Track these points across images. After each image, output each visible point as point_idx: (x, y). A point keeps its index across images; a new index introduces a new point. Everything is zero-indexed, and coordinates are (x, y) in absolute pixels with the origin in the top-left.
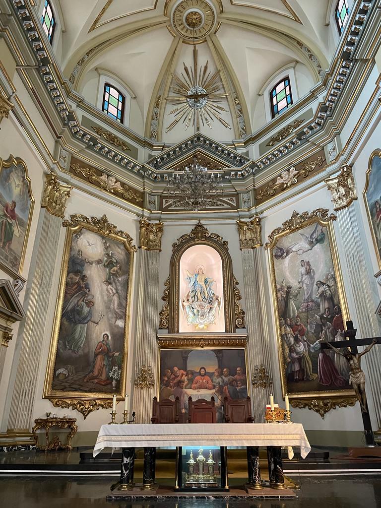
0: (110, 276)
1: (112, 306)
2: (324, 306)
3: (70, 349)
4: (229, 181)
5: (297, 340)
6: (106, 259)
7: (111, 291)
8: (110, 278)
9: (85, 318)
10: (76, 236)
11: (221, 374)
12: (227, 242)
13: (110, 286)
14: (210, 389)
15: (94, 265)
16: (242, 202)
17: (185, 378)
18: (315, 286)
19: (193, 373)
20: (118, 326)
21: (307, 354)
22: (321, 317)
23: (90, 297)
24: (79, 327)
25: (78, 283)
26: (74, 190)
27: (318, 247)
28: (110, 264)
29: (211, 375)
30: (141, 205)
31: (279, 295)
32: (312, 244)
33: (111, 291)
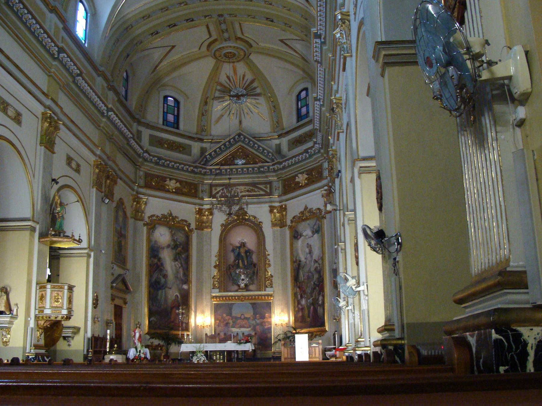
0: (176, 255)
1: (179, 276)
2: (316, 276)
3: (156, 306)
4: (263, 172)
5: (302, 297)
6: (172, 243)
7: (177, 266)
8: (176, 257)
9: (163, 286)
10: (152, 231)
11: (255, 318)
12: (262, 223)
13: (176, 263)
14: (247, 328)
15: (165, 249)
16: (274, 189)
17: (231, 321)
18: (313, 263)
19: (237, 318)
20: (184, 289)
21: (305, 306)
22: (314, 284)
23: (165, 272)
24: (160, 292)
25: (157, 264)
26: (150, 198)
27: (316, 236)
28: (175, 247)
29: (248, 319)
30: (195, 195)
31: (294, 266)
32: (313, 233)
33: (177, 266)
